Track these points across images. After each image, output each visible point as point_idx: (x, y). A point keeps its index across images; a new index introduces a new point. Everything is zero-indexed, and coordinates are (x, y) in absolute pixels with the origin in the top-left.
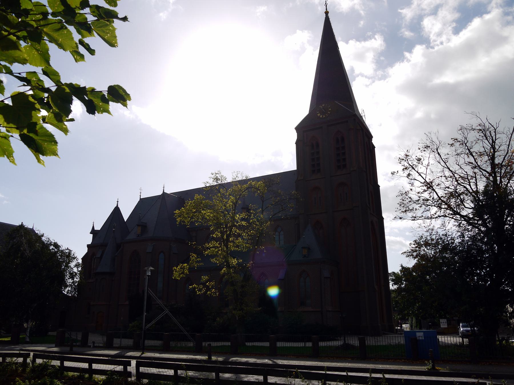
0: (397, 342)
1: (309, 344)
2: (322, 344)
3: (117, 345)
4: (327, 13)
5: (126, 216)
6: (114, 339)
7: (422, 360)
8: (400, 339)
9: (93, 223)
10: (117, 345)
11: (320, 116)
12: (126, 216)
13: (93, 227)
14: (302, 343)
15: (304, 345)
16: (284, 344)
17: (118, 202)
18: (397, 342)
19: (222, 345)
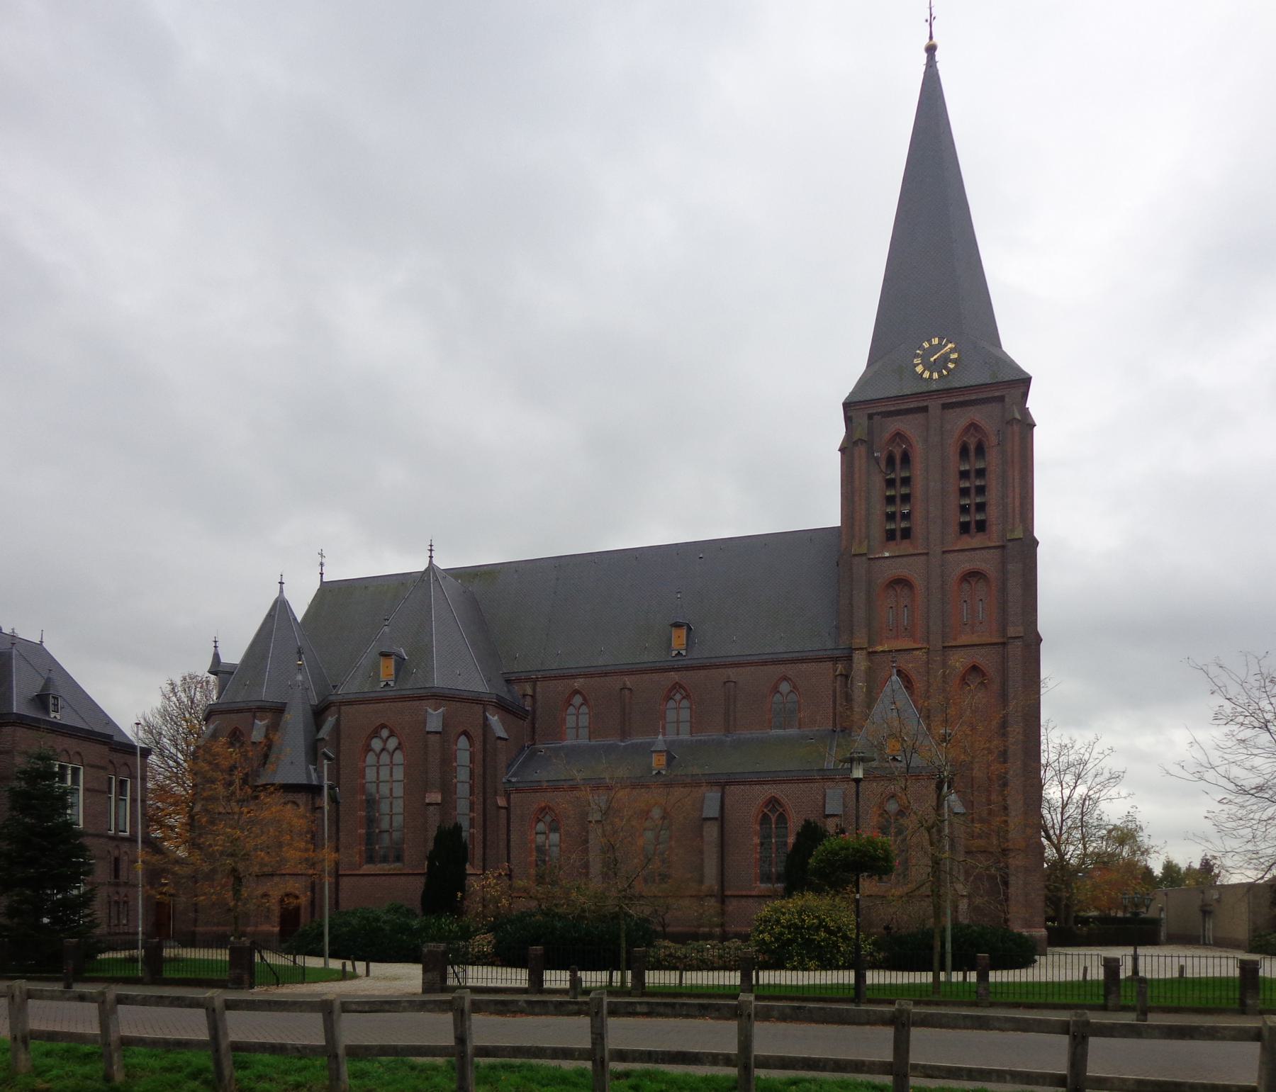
0: (657, 981)
1: (973, 977)
2: (995, 976)
3: (191, 974)
4: (931, 49)
5: (299, 610)
6: (647, 972)
7: (148, 887)
8: (1051, 972)
9: (215, 642)
10: (208, 974)
11: (923, 372)
12: (299, 610)
13: (216, 657)
14: (901, 973)
15: (961, 979)
16: (184, 954)
17: (281, 583)
18: (667, 982)
19: (1167, 976)
